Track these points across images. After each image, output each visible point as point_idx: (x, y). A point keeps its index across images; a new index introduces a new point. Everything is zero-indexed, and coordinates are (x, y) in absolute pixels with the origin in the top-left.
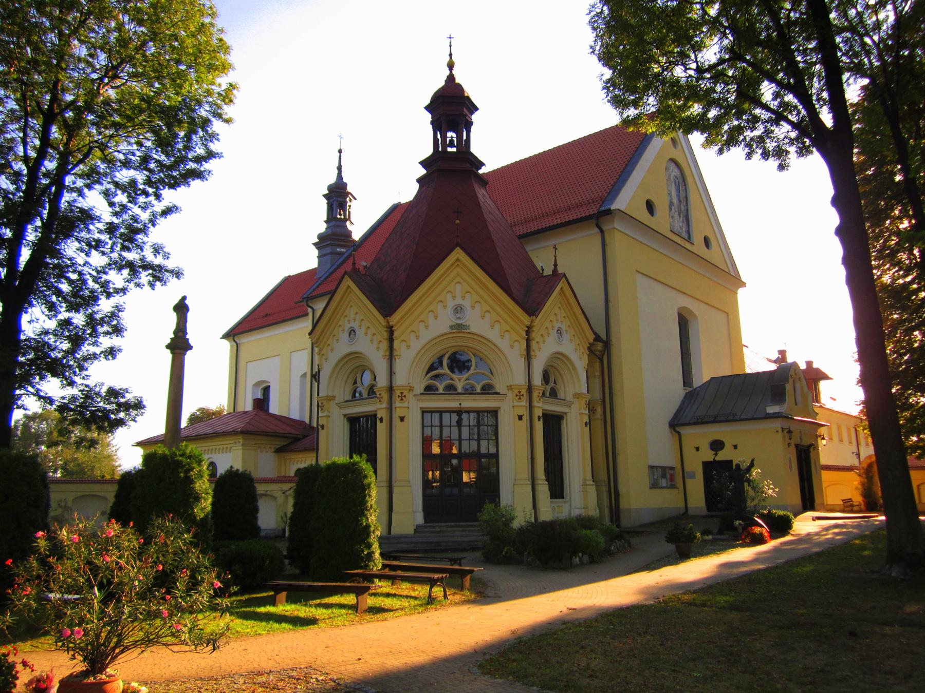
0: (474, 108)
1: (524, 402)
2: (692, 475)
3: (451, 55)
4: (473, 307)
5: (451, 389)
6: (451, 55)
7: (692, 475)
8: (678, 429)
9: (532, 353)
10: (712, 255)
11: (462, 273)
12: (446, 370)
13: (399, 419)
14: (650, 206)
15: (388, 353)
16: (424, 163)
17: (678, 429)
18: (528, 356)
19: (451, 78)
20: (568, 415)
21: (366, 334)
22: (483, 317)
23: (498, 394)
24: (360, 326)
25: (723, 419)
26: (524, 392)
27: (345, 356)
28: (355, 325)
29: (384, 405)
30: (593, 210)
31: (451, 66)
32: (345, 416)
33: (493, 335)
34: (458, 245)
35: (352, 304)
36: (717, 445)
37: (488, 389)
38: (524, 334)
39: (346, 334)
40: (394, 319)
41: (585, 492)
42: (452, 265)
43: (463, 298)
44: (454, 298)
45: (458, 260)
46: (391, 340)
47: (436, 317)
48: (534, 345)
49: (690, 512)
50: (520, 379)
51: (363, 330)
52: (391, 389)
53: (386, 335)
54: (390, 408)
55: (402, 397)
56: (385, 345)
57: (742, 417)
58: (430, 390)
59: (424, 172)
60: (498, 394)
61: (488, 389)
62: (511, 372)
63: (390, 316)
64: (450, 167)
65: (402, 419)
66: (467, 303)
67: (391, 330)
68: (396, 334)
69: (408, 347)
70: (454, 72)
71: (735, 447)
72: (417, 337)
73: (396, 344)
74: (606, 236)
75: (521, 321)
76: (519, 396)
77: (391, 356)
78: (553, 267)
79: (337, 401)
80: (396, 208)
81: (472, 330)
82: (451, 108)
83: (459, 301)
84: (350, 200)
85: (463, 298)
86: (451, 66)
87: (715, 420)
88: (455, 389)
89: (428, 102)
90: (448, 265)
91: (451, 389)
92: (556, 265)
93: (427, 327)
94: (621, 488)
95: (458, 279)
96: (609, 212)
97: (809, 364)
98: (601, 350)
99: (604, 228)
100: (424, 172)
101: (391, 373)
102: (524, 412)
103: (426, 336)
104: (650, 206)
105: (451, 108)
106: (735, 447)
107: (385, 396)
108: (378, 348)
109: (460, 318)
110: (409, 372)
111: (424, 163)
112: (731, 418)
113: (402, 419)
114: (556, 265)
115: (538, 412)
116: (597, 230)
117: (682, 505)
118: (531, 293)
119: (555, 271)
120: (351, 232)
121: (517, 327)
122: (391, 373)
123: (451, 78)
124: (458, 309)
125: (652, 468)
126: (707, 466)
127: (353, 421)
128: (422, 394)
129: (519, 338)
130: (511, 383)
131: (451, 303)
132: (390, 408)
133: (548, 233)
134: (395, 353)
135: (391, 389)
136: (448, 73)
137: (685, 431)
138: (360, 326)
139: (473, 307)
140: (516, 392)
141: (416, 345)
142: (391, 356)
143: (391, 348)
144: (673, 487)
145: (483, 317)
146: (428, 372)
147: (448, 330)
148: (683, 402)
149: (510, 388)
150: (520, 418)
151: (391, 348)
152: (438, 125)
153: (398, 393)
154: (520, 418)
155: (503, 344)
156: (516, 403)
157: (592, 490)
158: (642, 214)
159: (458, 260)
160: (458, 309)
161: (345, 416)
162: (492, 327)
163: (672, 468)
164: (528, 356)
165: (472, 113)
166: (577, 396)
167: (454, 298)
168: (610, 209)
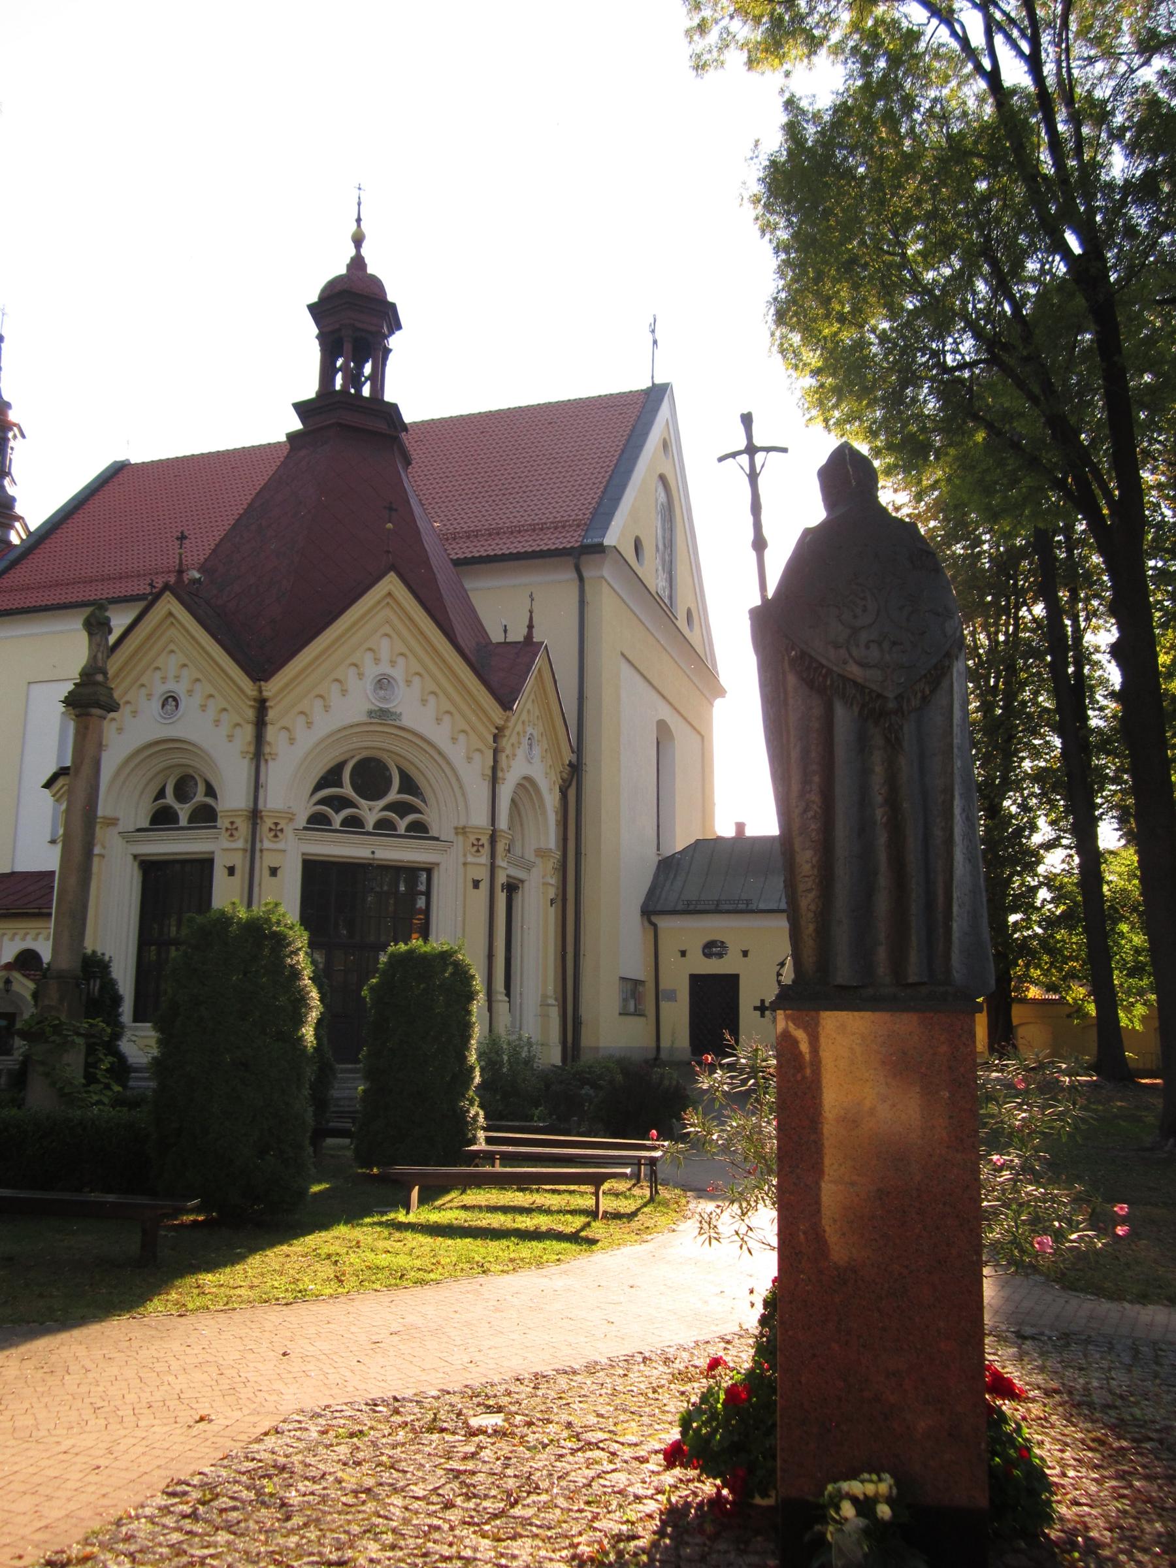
0: (312, 308)
1: (484, 859)
2: (672, 996)
3: (359, 220)
4: (408, 683)
5: (354, 823)
6: (359, 220)
7: (672, 996)
8: (654, 919)
9: (500, 774)
10: (694, 637)
11: (396, 621)
12: (347, 790)
13: (266, 872)
14: (638, 546)
15: (252, 749)
16: (302, 409)
17: (654, 919)
18: (494, 780)
19: (358, 263)
20: (526, 884)
21: (203, 707)
22: (424, 702)
23: (437, 839)
24: (190, 692)
25: (730, 907)
26: (485, 840)
27: (157, 743)
28: (180, 689)
29: (240, 844)
30: (569, 540)
31: (358, 240)
32: (135, 857)
33: (439, 735)
34: (393, 568)
35: (172, 647)
36: (713, 949)
37: (419, 829)
38: (491, 739)
39: (156, 704)
40: (271, 688)
41: (545, 1016)
42: (379, 602)
43: (393, 663)
44: (377, 661)
45: (389, 594)
46: (260, 724)
47: (344, 692)
48: (503, 758)
49: (664, 1055)
50: (479, 818)
51: (197, 699)
52: (255, 815)
53: (251, 714)
54: (252, 852)
55: (276, 832)
56: (249, 731)
57: (762, 906)
58: (318, 821)
59: (296, 425)
60: (437, 839)
61: (419, 829)
62: (461, 800)
63: (266, 680)
64: (348, 423)
65: (274, 872)
66: (398, 673)
67: (261, 706)
68: (271, 715)
69: (292, 741)
70: (363, 252)
71: (745, 954)
72: (309, 724)
73: (271, 733)
74: (587, 588)
75: (489, 719)
76: (477, 846)
77: (259, 753)
78: (525, 631)
79: (121, 828)
80: (807, 532)
81: (406, 722)
82: (354, 317)
83: (385, 668)
84: (15, 437)
85: (393, 663)
86: (358, 240)
87: (717, 909)
88: (362, 825)
89: (314, 298)
90: (371, 603)
91: (354, 823)
92: (530, 627)
93: (327, 708)
94: (585, 1013)
95: (387, 629)
96: (599, 549)
97: (740, 827)
98: (574, 777)
99: (585, 574)
100: (296, 425)
101: (257, 785)
102: (483, 874)
103: (325, 724)
104: (638, 546)
105: (354, 317)
106: (745, 954)
107: (243, 827)
108: (230, 737)
109: (385, 699)
110: (289, 789)
111: (302, 409)
112: (742, 906)
113: (274, 872)
114: (530, 627)
115: (501, 879)
116: (574, 575)
117: (653, 1044)
118: (501, 670)
119: (529, 637)
120: (13, 499)
121: (481, 728)
122: (257, 785)
123: (358, 263)
124: (383, 683)
125: (622, 979)
126: (697, 981)
127: (154, 873)
128: (305, 829)
129: (483, 748)
130: (462, 823)
131: (372, 671)
132: (252, 852)
133: (483, 566)
134: (267, 750)
135: (255, 815)
136: (353, 252)
137: (664, 923)
138: (190, 692)
139: (408, 683)
140: (472, 838)
141: (306, 740)
142: (259, 753)
143: (259, 739)
144: (639, 1013)
145: (424, 702)
146: (318, 787)
147: (365, 719)
148: (656, 876)
149: (462, 831)
150: (476, 884)
151: (259, 739)
152: (331, 345)
153: (269, 823)
154: (476, 884)
155: (456, 754)
156: (470, 859)
157: (554, 1013)
158: (629, 553)
159: (389, 594)
160: (383, 683)
161: (135, 857)
162: (439, 720)
163: (642, 982)
164: (494, 780)
165: (392, 333)
166: (541, 853)
167: (377, 661)
168: (601, 545)
